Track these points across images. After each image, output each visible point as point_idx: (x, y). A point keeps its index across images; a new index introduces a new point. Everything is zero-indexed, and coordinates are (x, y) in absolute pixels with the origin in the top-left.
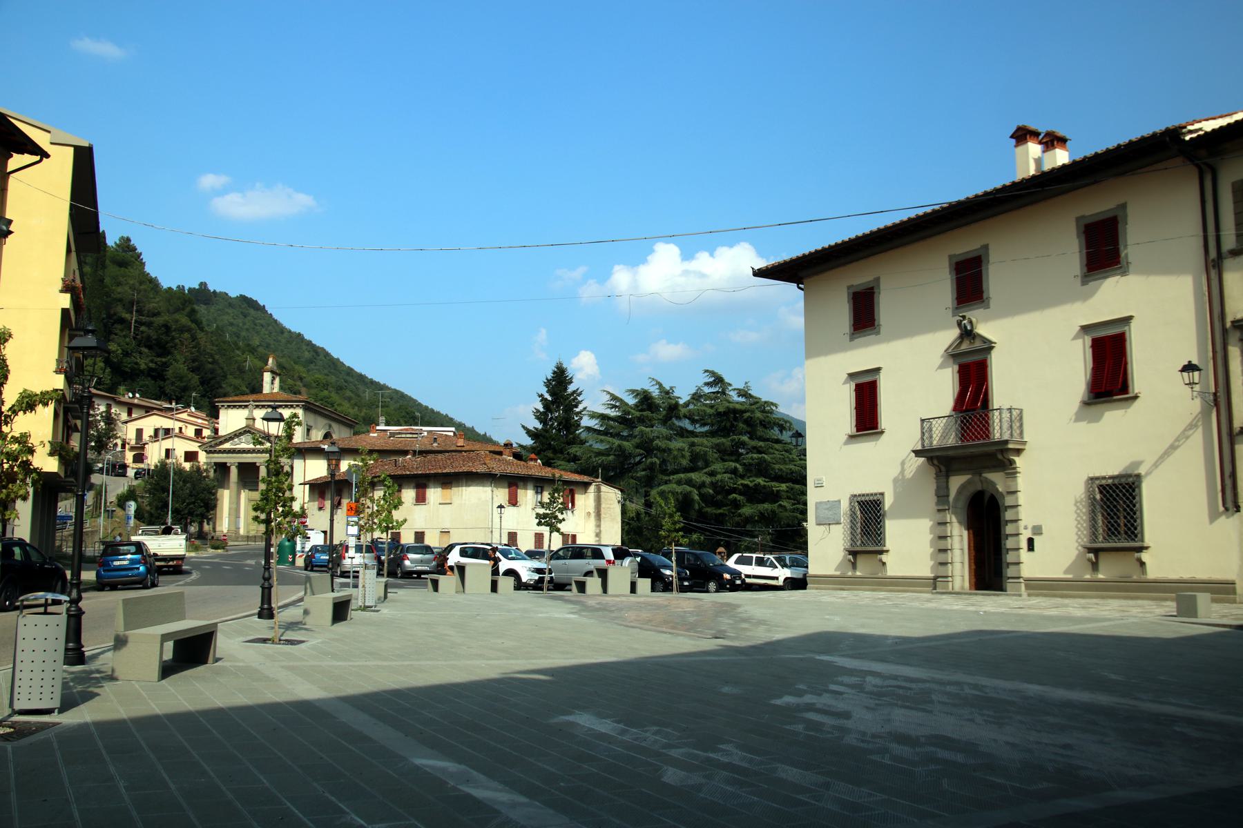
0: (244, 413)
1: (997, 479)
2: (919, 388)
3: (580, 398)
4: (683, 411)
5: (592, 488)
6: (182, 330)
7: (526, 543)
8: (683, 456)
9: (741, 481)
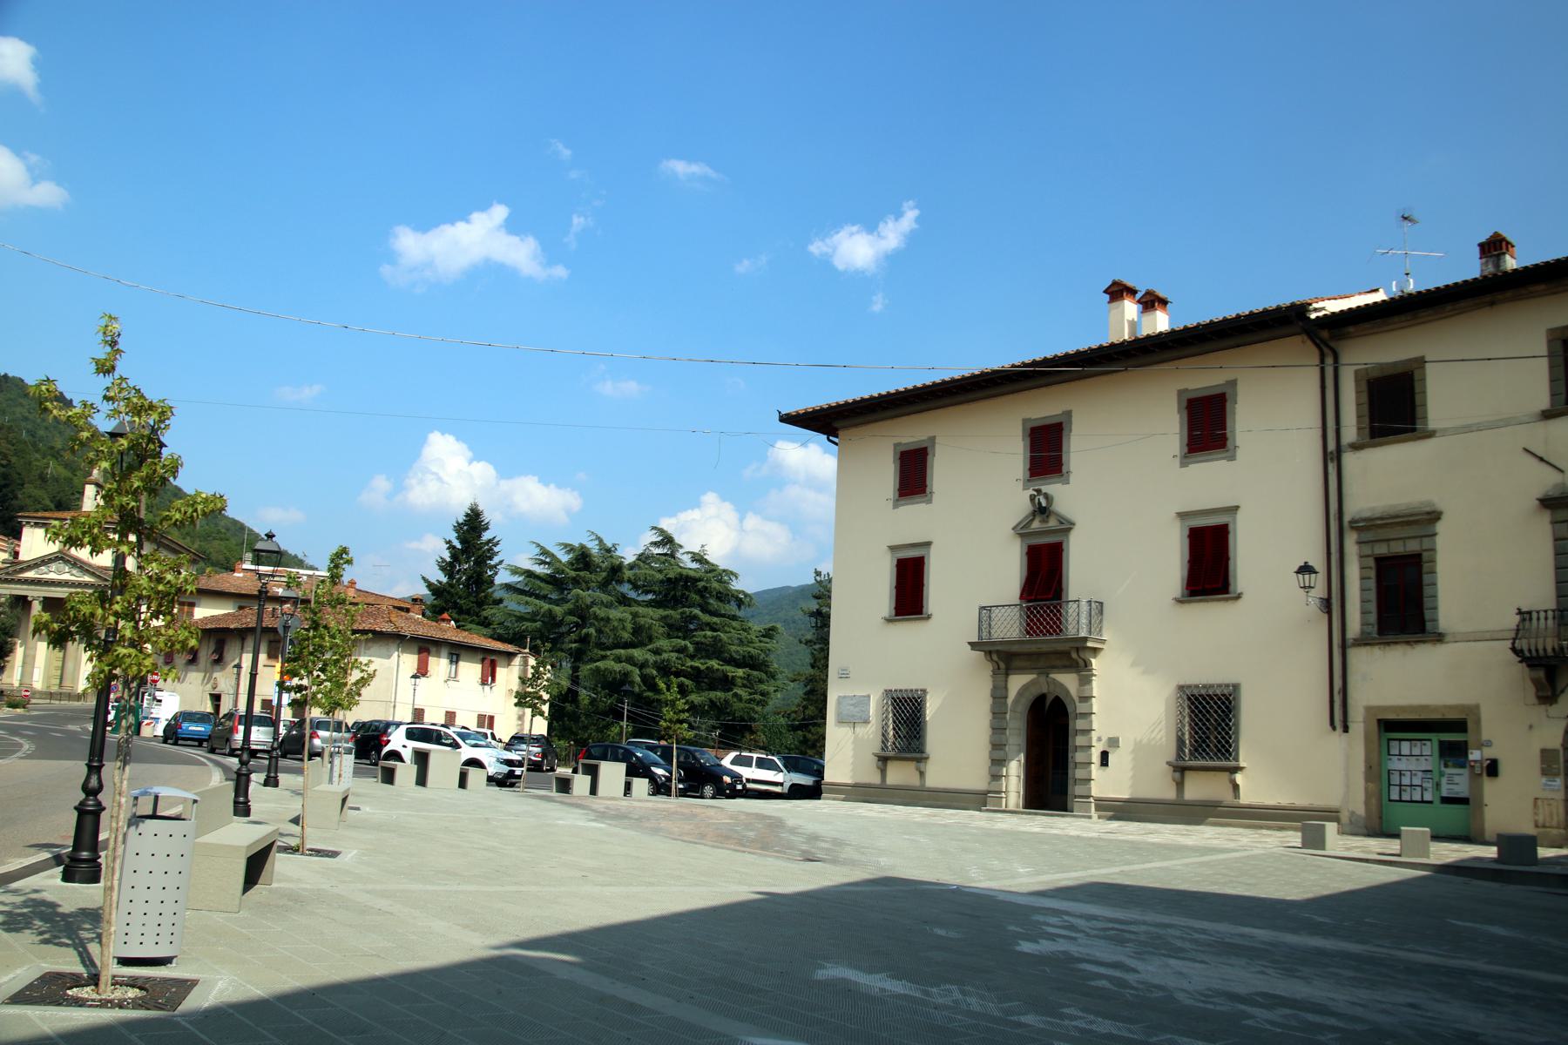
1: (1068, 680)
2: (978, 576)
3: (496, 549)
4: (628, 574)
5: (517, 660)
7: (505, 731)
8: (624, 628)
9: (690, 663)
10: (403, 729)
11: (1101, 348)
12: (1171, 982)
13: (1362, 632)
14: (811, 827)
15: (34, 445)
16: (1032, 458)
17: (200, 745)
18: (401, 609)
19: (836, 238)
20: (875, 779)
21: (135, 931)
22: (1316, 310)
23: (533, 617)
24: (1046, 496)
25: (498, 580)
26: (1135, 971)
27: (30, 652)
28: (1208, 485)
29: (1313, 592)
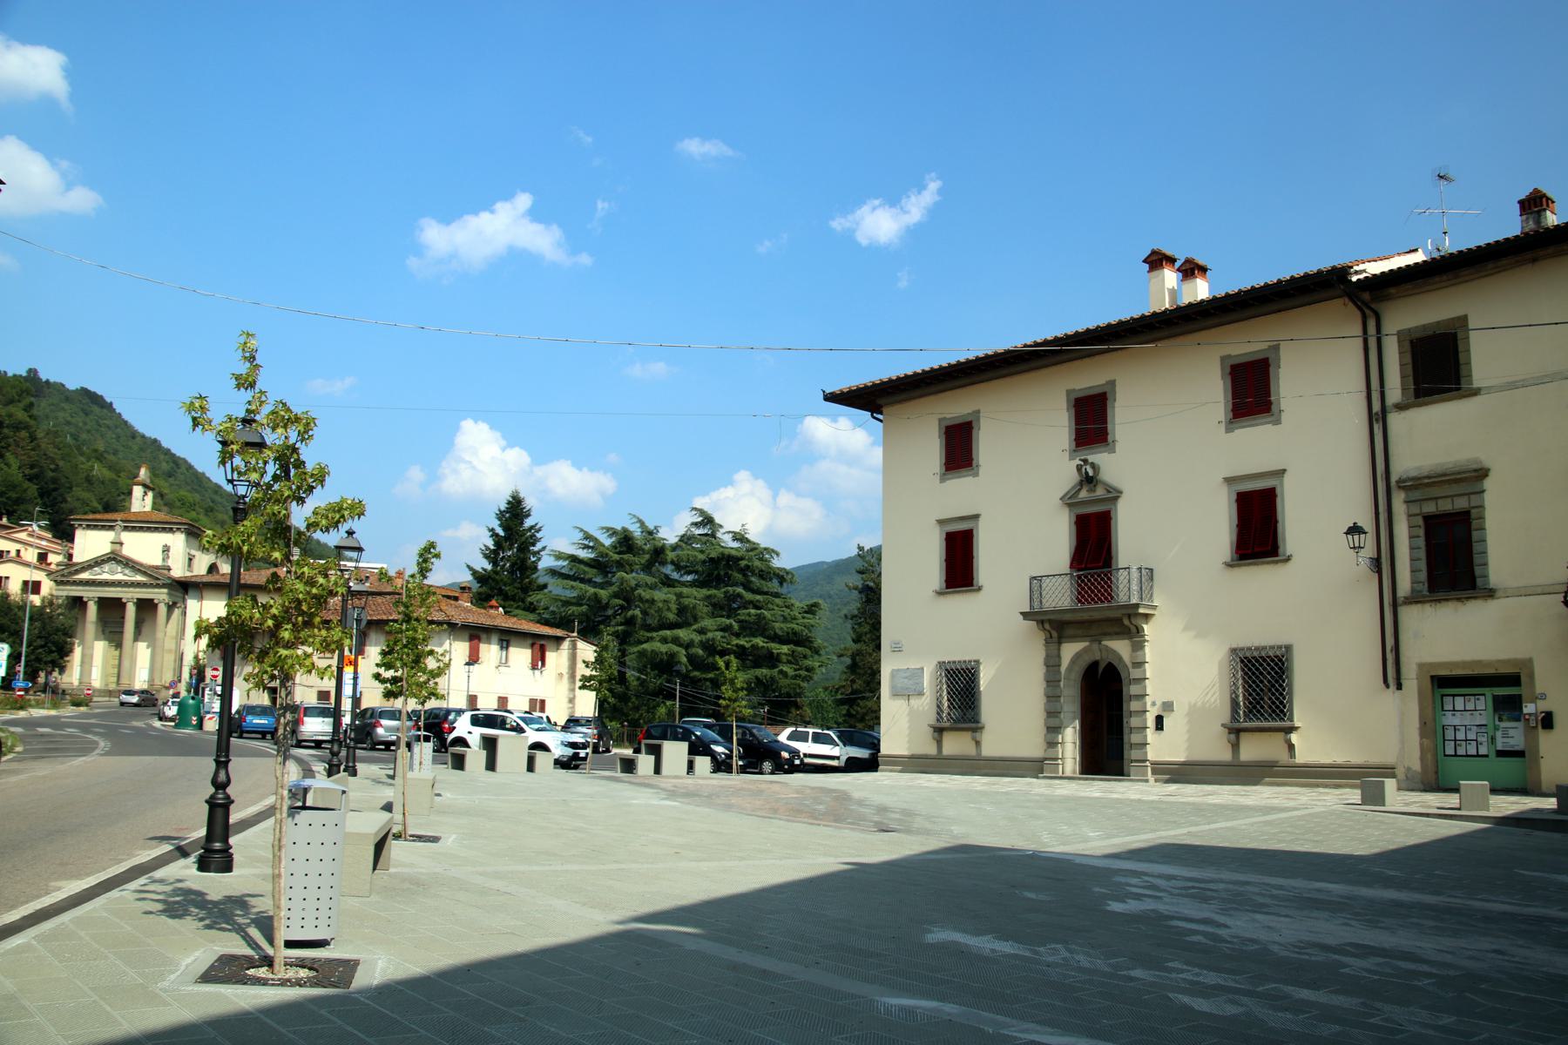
0: (109, 536)
1: (1121, 647)
2: (1027, 545)
4: (671, 555)
5: (566, 644)
6: (18, 426)
7: (559, 715)
8: (669, 609)
9: (735, 641)
10: (468, 715)
11: (1143, 317)
12: (1263, 936)
13: (1413, 590)
14: (879, 799)
15: (79, 448)
17: (264, 738)
18: (449, 597)
21: (296, 915)
22: (1357, 272)
23: (578, 601)
24: (1093, 466)
25: (542, 565)
26: (1226, 926)
28: (1254, 450)
29: (1362, 553)
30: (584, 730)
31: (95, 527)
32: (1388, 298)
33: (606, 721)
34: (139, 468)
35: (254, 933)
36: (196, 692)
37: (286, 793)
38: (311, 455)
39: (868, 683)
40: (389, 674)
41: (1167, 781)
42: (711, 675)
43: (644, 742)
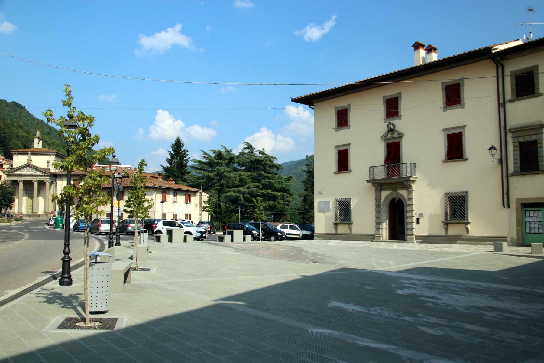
1: (403, 193)
2: (369, 155)
3: (187, 153)
4: (236, 160)
5: (198, 194)
8: (236, 180)
9: (261, 191)
10: (161, 222)
11: (412, 68)
12: (454, 303)
13: (514, 171)
14: (313, 250)
15: (13, 124)
16: (387, 112)
18: (154, 177)
19: (305, 29)
20: (334, 231)
21: (94, 302)
22: (495, 49)
23: (202, 178)
24: (393, 125)
25: (188, 164)
26: (441, 300)
27: (20, 201)
28: (454, 118)
29: (495, 157)
30: (205, 226)
31: (21, 154)
32: (507, 59)
33: (214, 222)
34: (36, 132)
35: (79, 309)
36: (61, 215)
37: (88, 258)
38: (93, 131)
39: (310, 206)
40: (129, 209)
41: (421, 243)
42: (252, 204)
43: (227, 230)
